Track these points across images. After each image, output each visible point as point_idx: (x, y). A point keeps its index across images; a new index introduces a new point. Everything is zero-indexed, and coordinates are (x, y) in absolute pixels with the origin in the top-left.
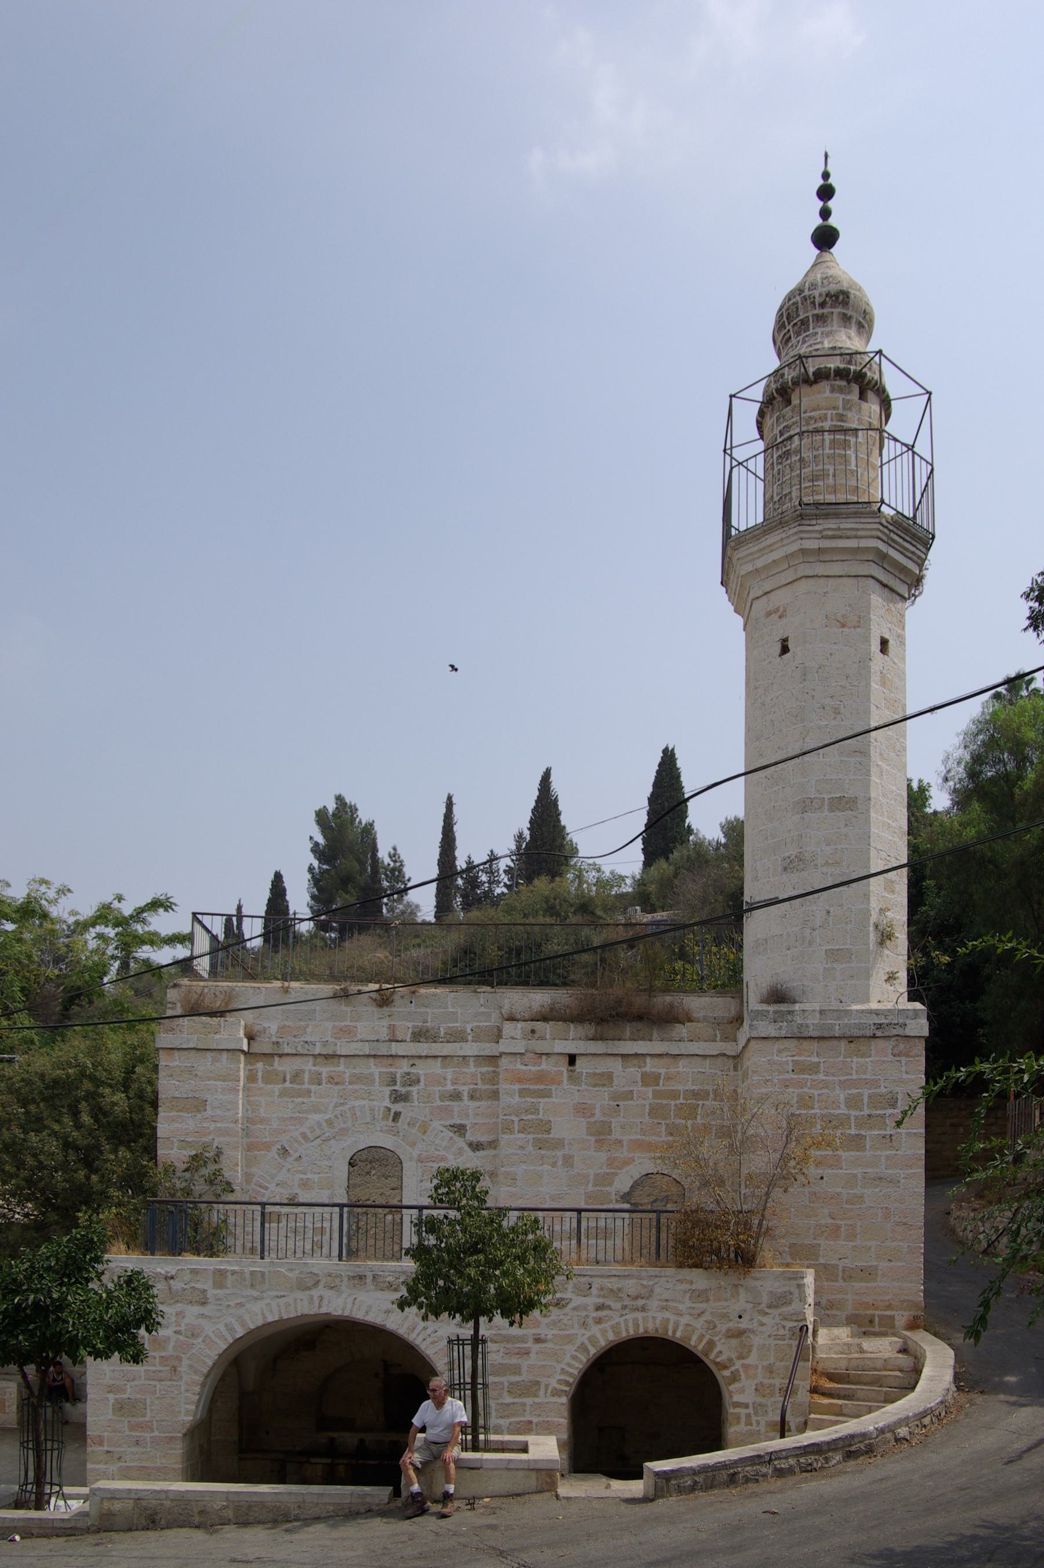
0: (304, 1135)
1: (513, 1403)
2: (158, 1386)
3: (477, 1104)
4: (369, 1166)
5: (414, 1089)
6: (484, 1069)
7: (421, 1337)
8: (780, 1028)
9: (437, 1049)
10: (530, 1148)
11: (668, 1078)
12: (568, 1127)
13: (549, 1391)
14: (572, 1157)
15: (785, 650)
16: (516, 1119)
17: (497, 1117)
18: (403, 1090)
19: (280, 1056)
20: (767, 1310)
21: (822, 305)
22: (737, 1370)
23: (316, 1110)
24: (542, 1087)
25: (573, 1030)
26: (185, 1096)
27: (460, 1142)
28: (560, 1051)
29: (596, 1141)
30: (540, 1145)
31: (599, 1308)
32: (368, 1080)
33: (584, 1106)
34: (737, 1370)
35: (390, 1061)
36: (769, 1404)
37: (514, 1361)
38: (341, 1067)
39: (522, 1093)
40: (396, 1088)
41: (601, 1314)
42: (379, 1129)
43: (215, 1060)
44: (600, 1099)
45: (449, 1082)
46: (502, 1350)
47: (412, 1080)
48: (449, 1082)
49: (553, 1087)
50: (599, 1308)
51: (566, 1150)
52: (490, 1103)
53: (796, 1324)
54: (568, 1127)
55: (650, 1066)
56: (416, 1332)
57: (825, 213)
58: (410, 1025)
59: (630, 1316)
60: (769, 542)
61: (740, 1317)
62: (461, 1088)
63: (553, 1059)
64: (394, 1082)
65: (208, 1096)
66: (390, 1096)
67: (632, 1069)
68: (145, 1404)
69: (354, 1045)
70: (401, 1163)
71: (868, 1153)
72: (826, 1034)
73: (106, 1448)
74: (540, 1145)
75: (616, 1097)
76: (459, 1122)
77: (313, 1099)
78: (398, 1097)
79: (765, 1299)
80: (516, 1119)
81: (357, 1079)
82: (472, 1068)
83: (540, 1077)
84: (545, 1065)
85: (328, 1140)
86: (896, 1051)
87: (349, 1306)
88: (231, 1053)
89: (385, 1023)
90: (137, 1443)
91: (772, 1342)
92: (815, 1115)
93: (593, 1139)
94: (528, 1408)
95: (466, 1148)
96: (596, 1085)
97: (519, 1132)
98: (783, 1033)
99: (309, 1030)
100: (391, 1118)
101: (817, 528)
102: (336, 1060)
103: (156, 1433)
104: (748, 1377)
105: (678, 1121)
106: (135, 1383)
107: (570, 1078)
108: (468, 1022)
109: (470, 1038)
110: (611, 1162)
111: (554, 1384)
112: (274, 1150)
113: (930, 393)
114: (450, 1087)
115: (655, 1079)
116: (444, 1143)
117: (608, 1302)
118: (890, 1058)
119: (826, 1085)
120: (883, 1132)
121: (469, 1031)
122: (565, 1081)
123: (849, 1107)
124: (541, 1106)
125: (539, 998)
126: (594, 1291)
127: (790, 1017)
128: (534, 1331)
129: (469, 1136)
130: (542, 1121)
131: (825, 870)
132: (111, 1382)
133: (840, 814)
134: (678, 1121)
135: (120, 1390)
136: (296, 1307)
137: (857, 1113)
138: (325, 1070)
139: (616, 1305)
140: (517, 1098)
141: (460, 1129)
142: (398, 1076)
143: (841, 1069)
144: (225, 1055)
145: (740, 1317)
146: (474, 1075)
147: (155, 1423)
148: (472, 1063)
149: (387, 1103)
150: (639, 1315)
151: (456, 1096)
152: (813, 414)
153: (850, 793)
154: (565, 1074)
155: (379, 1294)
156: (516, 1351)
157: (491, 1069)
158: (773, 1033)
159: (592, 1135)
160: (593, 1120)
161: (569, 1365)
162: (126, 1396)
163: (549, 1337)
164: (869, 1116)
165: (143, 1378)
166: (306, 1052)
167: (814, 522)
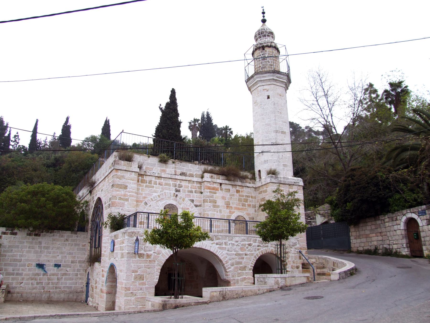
0: (152, 199)
3: (197, 194)
5: (181, 189)
7: (220, 253)
10: (212, 207)
11: (242, 192)
12: (220, 203)
18: (178, 189)
19: (146, 175)
21: (269, 33)
23: (156, 192)
25: (221, 177)
27: (193, 205)
30: (214, 206)
31: (258, 246)
32: (169, 185)
35: (175, 180)
37: (241, 260)
38: (162, 181)
39: (210, 192)
41: (259, 247)
43: (130, 174)
44: (228, 195)
47: (180, 186)
50: (258, 246)
54: (220, 203)
55: (238, 188)
57: (264, 17)
59: (265, 248)
62: (193, 190)
63: (217, 184)
64: (176, 186)
65: (128, 185)
69: (166, 175)
73: (131, 291)
74: (214, 206)
78: (177, 191)
81: (166, 184)
82: (195, 185)
83: (214, 189)
84: (215, 185)
85: (158, 201)
87: (201, 245)
89: (174, 170)
90: (141, 289)
91: (293, 255)
98: (277, 182)
99: (154, 169)
102: (161, 178)
103: (147, 286)
104: (289, 264)
107: (221, 189)
111: (250, 267)
112: (143, 203)
114: (190, 189)
116: (189, 204)
117: (260, 245)
125: (210, 168)
126: (257, 241)
128: (245, 252)
129: (195, 203)
132: (134, 269)
135: (136, 272)
138: (158, 181)
139: (262, 245)
141: (192, 201)
144: (133, 173)
146: (196, 186)
149: (174, 192)
150: (266, 248)
151: (191, 192)
155: (209, 242)
162: (138, 274)
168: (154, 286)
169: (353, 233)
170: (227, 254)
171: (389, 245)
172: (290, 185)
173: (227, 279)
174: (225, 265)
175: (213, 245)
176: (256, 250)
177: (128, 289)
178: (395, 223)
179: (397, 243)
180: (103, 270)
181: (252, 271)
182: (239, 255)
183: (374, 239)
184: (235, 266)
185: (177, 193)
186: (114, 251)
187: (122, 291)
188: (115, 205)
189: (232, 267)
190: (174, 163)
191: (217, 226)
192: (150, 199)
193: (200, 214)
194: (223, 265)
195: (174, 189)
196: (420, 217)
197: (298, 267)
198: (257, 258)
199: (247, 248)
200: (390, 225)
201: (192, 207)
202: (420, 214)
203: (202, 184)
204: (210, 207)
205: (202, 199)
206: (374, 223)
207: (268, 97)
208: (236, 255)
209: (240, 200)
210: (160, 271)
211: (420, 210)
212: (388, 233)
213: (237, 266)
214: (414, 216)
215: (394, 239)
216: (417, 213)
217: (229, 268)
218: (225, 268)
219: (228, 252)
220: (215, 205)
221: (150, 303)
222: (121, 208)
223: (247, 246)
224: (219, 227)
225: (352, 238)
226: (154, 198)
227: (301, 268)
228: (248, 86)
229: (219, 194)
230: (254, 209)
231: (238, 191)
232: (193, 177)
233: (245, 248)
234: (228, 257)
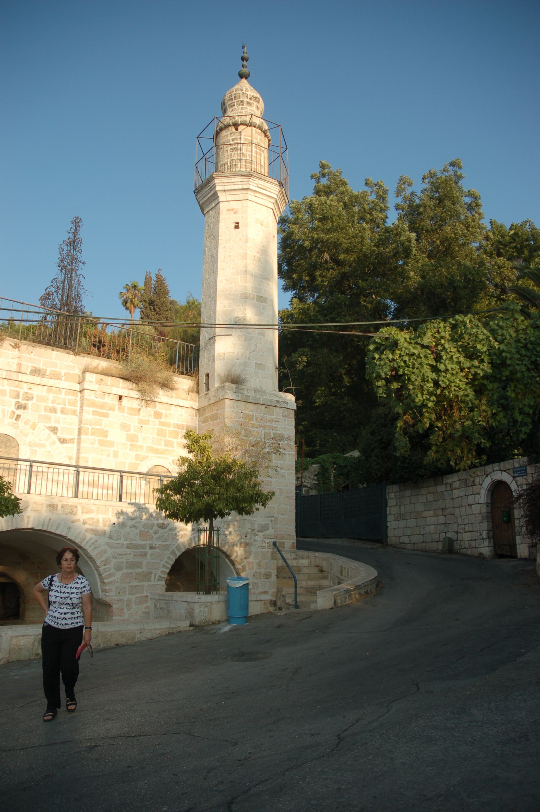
1: (138, 586)
5: (30, 403)
8: (238, 396)
9: (45, 381)
10: (96, 445)
11: (166, 416)
15: (237, 227)
18: (23, 402)
20: (257, 533)
21: (250, 99)
22: (245, 565)
27: (54, 437)
29: (131, 445)
30: (101, 443)
34: (245, 565)
39: (95, 413)
45: (50, 401)
46: (132, 553)
47: (28, 397)
48: (50, 401)
53: (270, 540)
54: (116, 435)
58: (30, 365)
60: (233, 181)
62: (56, 406)
64: (18, 396)
66: (16, 404)
75: (141, 422)
78: (19, 406)
79: (256, 527)
80: (90, 427)
82: (63, 396)
86: (284, 415)
89: (16, 361)
91: (260, 550)
93: (129, 443)
96: (131, 415)
97: (91, 435)
98: (239, 398)
100: (15, 418)
105: (170, 439)
107: (119, 408)
109: (63, 378)
110: (137, 457)
111: (159, 573)
114: (50, 405)
118: (281, 417)
125: (103, 364)
128: (150, 542)
129: (59, 434)
136: (12, 523)
141: (54, 430)
149: (13, 408)
157: (74, 398)
160: (129, 433)
167: (255, 179)
169: (393, 509)
170: (108, 544)
171: (457, 533)
172: (267, 406)
173: (105, 599)
174: (101, 569)
178: (470, 490)
179: (471, 529)
181: (163, 583)
183: (430, 521)
189: (119, 574)
190: (16, 346)
193: (70, 458)
195: (14, 403)
196: (517, 478)
198: (178, 554)
200: (462, 494)
201: (54, 443)
202: (517, 474)
204: (92, 443)
206: (432, 489)
208: (128, 547)
209: (160, 433)
211: (517, 465)
212: (457, 510)
214: (506, 477)
215: (466, 521)
216: (511, 472)
217: (110, 576)
218: (100, 575)
219: (111, 541)
223: (156, 528)
225: (389, 518)
227: (274, 578)
228: (199, 203)
229: (116, 418)
234: (110, 552)
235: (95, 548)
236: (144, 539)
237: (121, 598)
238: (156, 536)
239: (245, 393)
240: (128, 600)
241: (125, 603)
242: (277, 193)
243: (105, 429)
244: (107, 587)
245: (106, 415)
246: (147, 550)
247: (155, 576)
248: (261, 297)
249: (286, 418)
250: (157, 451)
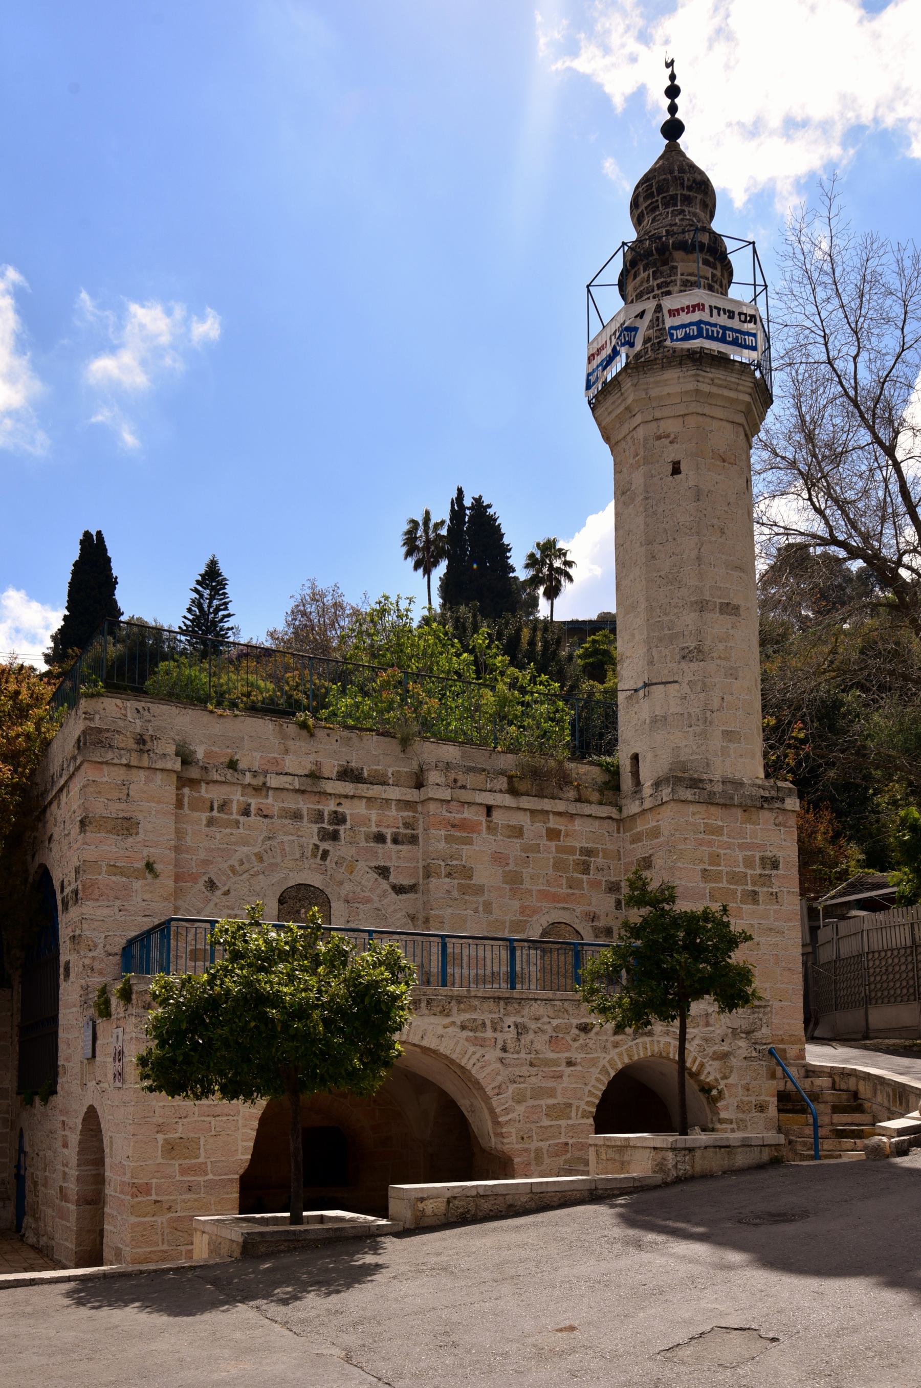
0: (232, 869)
1: (551, 1126)
2: (213, 1123)
3: (400, 847)
4: (298, 905)
5: (341, 828)
6: (406, 814)
7: (472, 1061)
8: (695, 794)
10: (455, 893)
11: (567, 835)
13: (580, 1113)
14: (490, 904)
16: (442, 863)
17: (418, 862)
23: (245, 843)
24: (465, 835)
26: (114, 816)
27: (385, 885)
28: (480, 801)
29: (511, 890)
30: (464, 890)
33: (500, 855)
36: (748, 1119)
37: (550, 1084)
39: (449, 839)
40: (324, 825)
42: (307, 866)
43: (148, 780)
44: (514, 848)
45: (373, 824)
47: (338, 818)
49: (475, 835)
51: (486, 897)
52: (410, 847)
54: (486, 875)
56: (467, 1057)
61: (723, 1041)
62: (384, 830)
63: (474, 809)
66: (319, 832)
67: (538, 824)
68: (198, 1143)
70: (329, 902)
71: (761, 907)
72: (728, 802)
73: (154, 1197)
76: (382, 864)
77: (241, 830)
82: (393, 812)
84: (467, 814)
86: (777, 821)
88: (165, 774)
92: (722, 871)
94: (563, 1130)
95: (390, 890)
96: (509, 837)
101: (710, 375)
103: (210, 1176)
106: (188, 1120)
107: (488, 828)
108: (389, 767)
110: (523, 910)
111: (584, 1106)
113: (754, 243)
114: (374, 829)
115: (553, 834)
116: (370, 885)
118: (773, 827)
119: (729, 846)
120: (770, 890)
121: (390, 775)
122: (484, 829)
123: (746, 866)
124: (464, 852)
127: (701, 785)
128: (567, 1055)
129: (392, 879)
130: (464, 867)
131: (719, 662)
133: (728, 617)
134: (576, 875)
137: (752, 872)
138: (254, 802)
140: (443, 844)
141: (384, 872)
142: (326, 814)
143: (739, 833)
145: (723, 1041)
147: (209, 1164)
148: (394, 807)
149: (315, 840)
151: (380, 838)
152: (689, 278)
153: (735, 602)
154: (484, 824)
155: (433, 1019)
156: (552, 1074)
157: (411, 814)
158: (690, 798)
159: (507, 883)
161: (594, 1086)
162: (177, 1136)
163: (579, 1060)
164: (760, 875)
165: (196, 1115)
166: (235, 781)
167: (708, 370)
168: (237, 1177)
174: (494, 1102)
175: (451, 1030)
176: (609, 1045)
177: (144, 1189)
180: (63, 1122)
182: (547, 1063)
184: (531, 1102)
185: (324, 846)
186: (94, 1056)
187: (123, 1196)
188: (97, 892)
191: (473, 962)
192: (225, 866)
194: (487, 1099)
197: (761, 1108)
198: (613, 1074)
199: (575, 1040)
201: (384, 895)
203: (420, 808)
205: (420, 865)
207: (676, 469)
208: (531, 1065)
209: (559, 865)
210: (256, 1124)
213: (536, 1103)
217: (507, 1111)
218: (492, 1111)
220: (469, 886)
221: (206, 1237)
222: (118, 903)
224: (481, 962)
226: (242, 863)
227: (772, 1111)
230: (611, 900)
231: (553, 834)
232: (384, 783)
233: (568, 1038)
235: (482, 1067)
236: (557, 1050)
237: (527, 1146)
238: (577, 1044)
239: (708, 787)
240: (536, 1149)
241: (533, 1155)
242: (749, 390)
243: (468, 865)
244: (504, 1130)
245: (469, 841)
246: (563, 1068)
247: (577, 1110)
248: (728, 604)
249: (782, 828)
250: (555, 898)
